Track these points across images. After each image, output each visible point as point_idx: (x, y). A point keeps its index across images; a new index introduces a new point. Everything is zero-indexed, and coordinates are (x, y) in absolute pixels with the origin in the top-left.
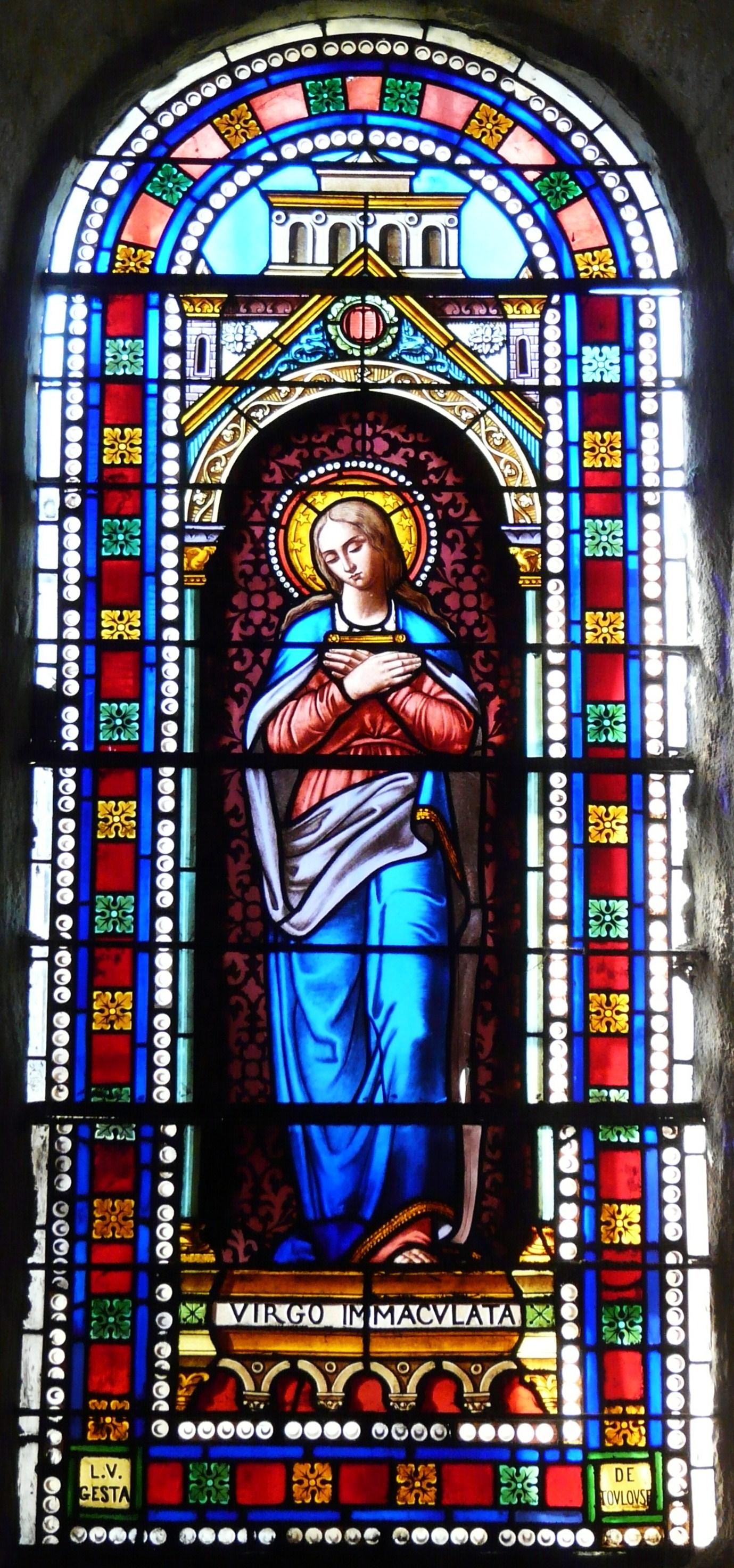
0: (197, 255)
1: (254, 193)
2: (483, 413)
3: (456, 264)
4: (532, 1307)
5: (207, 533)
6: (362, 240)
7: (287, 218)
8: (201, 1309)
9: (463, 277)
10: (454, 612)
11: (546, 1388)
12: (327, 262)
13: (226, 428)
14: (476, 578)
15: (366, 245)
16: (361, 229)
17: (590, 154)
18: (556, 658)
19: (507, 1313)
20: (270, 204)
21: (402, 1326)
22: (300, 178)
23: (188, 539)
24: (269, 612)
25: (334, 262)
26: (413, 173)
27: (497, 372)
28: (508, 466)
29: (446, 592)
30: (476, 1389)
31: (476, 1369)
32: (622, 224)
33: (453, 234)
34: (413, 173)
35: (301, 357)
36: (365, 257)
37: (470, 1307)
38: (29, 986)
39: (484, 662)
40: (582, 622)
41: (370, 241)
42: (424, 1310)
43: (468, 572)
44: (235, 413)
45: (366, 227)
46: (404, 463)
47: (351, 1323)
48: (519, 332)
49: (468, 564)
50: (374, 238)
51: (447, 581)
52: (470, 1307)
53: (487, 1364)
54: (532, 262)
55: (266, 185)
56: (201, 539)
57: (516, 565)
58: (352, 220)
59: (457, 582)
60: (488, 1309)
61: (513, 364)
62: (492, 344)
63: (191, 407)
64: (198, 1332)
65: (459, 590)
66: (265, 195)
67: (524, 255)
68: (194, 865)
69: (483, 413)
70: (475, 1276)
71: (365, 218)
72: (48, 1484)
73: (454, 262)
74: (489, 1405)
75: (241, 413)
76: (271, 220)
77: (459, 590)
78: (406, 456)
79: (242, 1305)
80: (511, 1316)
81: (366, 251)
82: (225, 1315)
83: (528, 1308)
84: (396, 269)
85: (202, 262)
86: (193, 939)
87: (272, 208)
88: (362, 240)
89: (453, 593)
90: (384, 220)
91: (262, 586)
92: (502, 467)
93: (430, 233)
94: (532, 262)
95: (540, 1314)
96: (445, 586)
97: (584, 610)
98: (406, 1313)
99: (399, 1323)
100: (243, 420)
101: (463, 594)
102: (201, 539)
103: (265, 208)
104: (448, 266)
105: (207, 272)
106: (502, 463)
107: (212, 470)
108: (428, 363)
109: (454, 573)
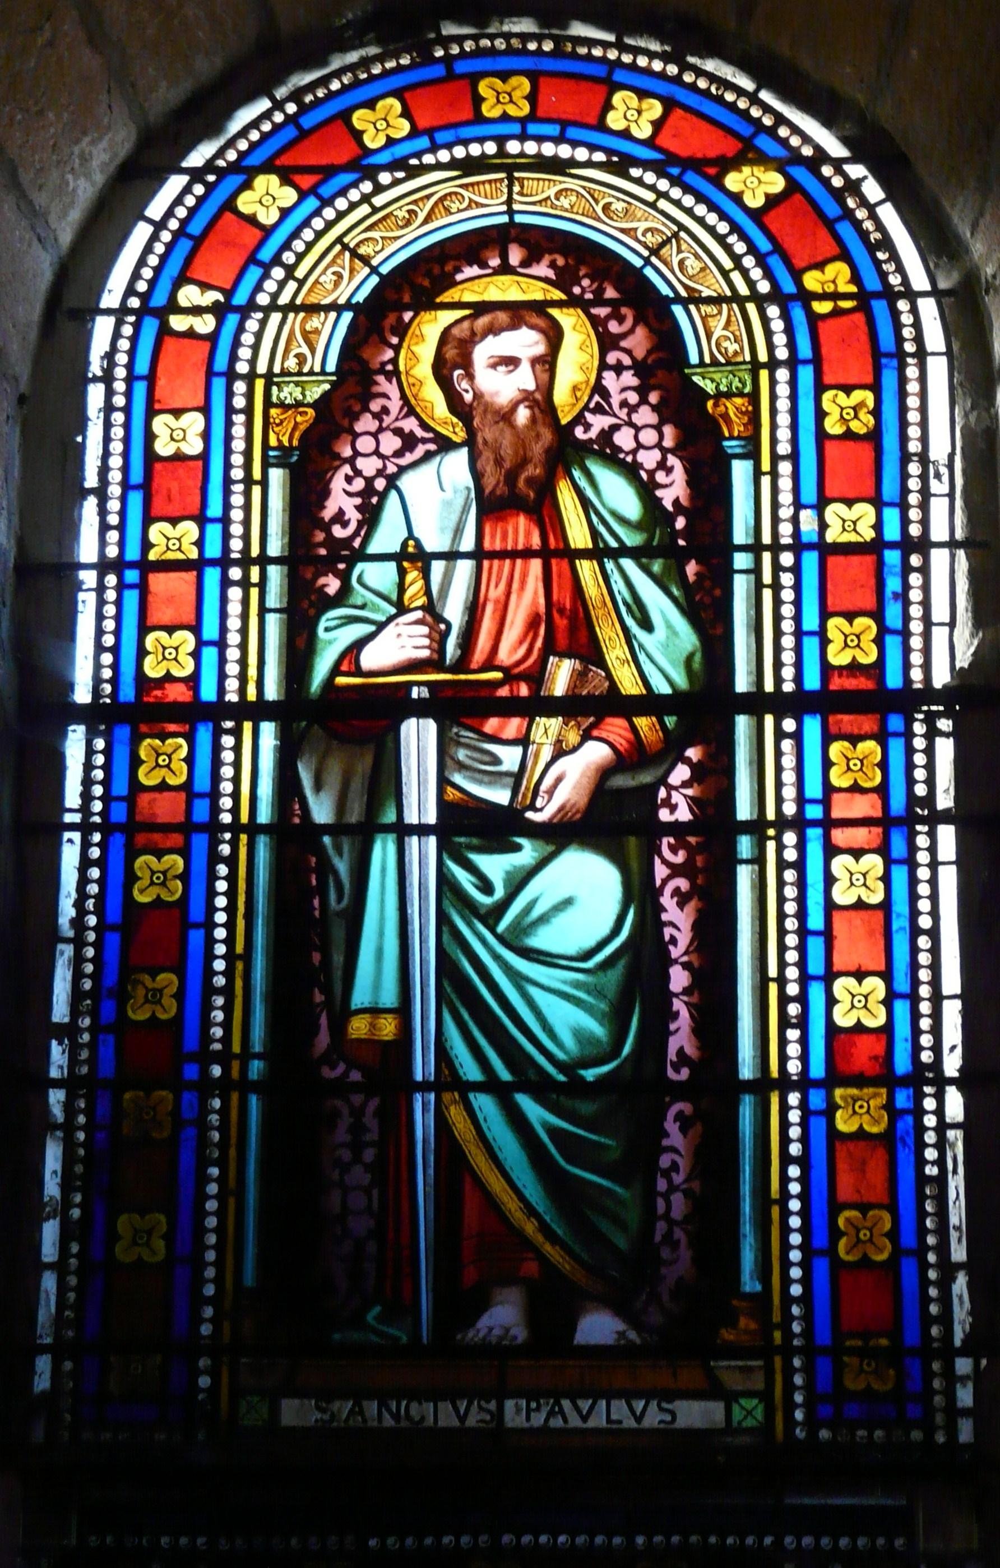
14: (654, 408)
39: (673, 849)
43: (644, 400)
46: (551, 274)
49: (643, 391)
51: (615, 416)
59: (629, 415)
65: (630, 424)
68: (285, 605)
78: (552, 265)
86: (286, 554)
91: (372, 425)
100: (347, 254)
109: (624, 404)
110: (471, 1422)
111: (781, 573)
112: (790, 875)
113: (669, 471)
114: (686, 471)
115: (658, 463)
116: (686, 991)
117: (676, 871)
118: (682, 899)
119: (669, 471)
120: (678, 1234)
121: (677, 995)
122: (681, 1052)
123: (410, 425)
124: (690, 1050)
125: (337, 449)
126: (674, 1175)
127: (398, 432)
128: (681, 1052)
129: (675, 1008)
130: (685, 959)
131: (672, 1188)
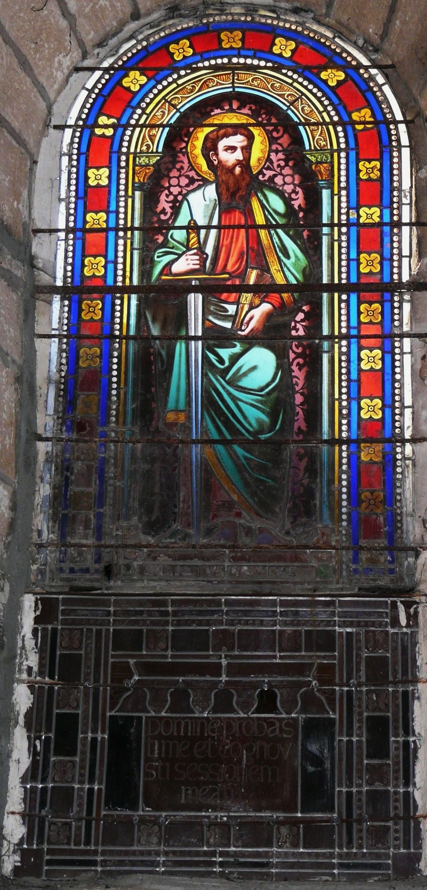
10: (280, 186)
18: (344, 230)
24: (281, 174)
29: (275, 176)
38: (35, 351)
40: (358, 261)
43: (287, 165)
46: (249, 112)
49: (286, 161)
59: (281, 170)
65: (180, 187)
70: (215, 872)
77: (180, 187)
89: (279, 176)
91: (177, 174)
96: (274, 173)
97: (359, 254)
101: (284, 176)
109: (279, 166)
112: (343, 305)
117: (298, 356)
122: (299, 428)
123: (192, 174)
125: (162, 183)
127: (187, 177)
128: (299, 428)
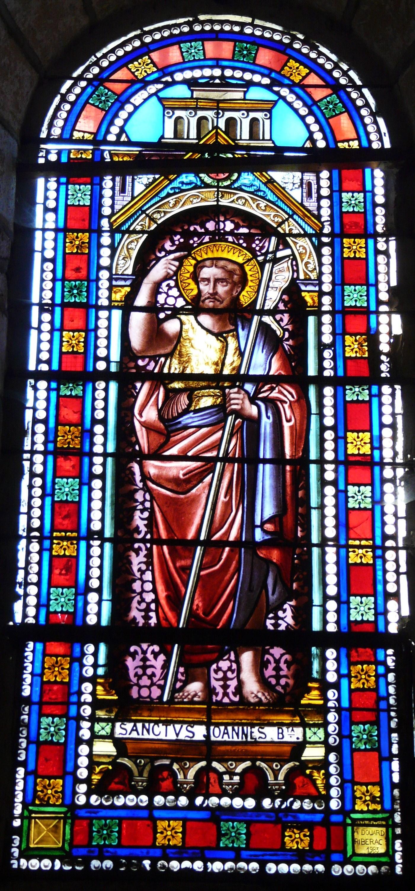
0: (122, 130)
1: (154, 98)
2: (287, 220)
3: (269, 138)
4: (310, 729)
5: (125, 280)
6: (215, 125)
7: (173, 113)
8: (108, 726)
9: (273, 145)
11: (319, 777)
12: (195, 137)
13: (138, 224)
15: (216, 128)
16: (215, 120)
17: (343, 81)
19: (226, 731)
20: (163, 105)
21: (131, 736)
22: (182, 91)
23: (114, 283)
25: (199, 138)
26: (245, 89)
27: (296, 198)
28: (302, 248)
30: (276, 778)
31: (277, 766)
32: (362, 118)
33: (267, 122)
34: (245, 89)
35: (182, 186)
36: (217, 134)
37: (132, 724)
41: (219, 125)
42: (156, 726)
44: (144, 215)
45: (217, 118)
47: (233, 738)
48: (308, 178)
50: (222, 124)
52: (132, 724)
53: (237, 763)
54: (311, 138)
55: (161, 95)
56: (122, 283)
57: (306, 302)
58: (210, 114)
60: (165, 727)
61: (304, 194)
62: (294, 184)
63: (118, 212)
64: (107, 740)
66: (160, 100)
67: (307, 135)
69: (287, 220)
71: (218, 114)
72: (338, 806)
73: (267, 137)
74: (284, 787)
75: (147, 215)
76: (164, 115)
79: (179, 726)
80: (136, 730)
81: (217, 131)
82: (119, 732)
83: (307, 729)
84: (233, 140)
85: (124, 135)
87: (165, 108)
88: (215, 125)
90: (228, 115)
92: (298, 248)
93: (254, 122)
94: (311, 138)
95: (315, 733)
98: (135, 728)
99: (130, 734)
102: (122, 283)
103: (161, 108)
104: (263, 139)
105: (126, 140)
106: (298, 246)
107: (129, 247)
108: (256, 191)
110: (182, 737)
111: (74, 138)
113: (139, 570)
114: (129, 676)
115: (144, 574)
116: (136, 491)
118: (137, 530)
119: (139, 570)
120: (138, 575)
121: (141, 489)
122: (138, 555)
124: (133, 554)
126: (140, 600)
128: (138, 555)
129: (142, 483)
130: (134, 595)
131: (142, 503)
